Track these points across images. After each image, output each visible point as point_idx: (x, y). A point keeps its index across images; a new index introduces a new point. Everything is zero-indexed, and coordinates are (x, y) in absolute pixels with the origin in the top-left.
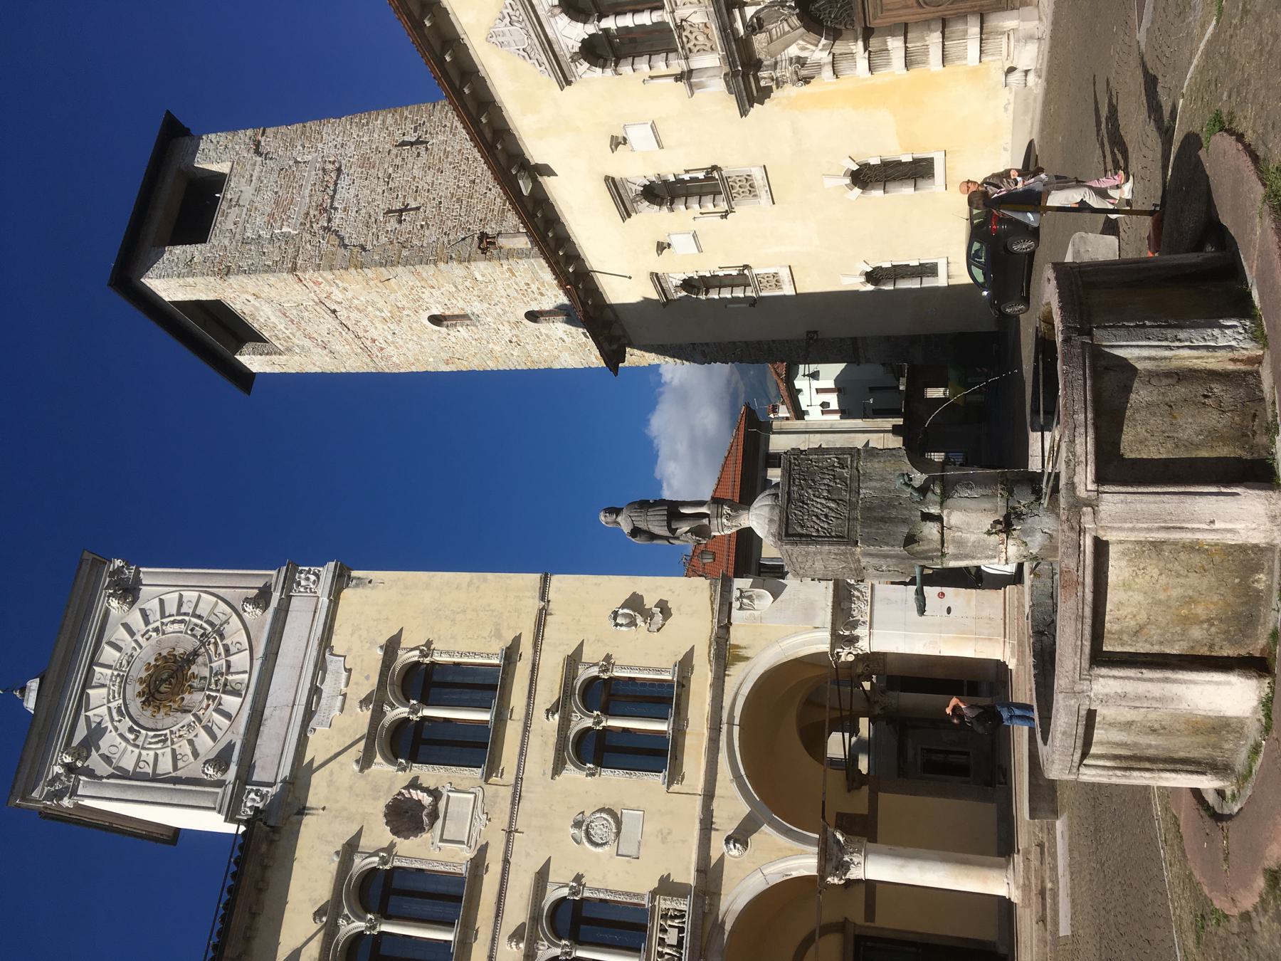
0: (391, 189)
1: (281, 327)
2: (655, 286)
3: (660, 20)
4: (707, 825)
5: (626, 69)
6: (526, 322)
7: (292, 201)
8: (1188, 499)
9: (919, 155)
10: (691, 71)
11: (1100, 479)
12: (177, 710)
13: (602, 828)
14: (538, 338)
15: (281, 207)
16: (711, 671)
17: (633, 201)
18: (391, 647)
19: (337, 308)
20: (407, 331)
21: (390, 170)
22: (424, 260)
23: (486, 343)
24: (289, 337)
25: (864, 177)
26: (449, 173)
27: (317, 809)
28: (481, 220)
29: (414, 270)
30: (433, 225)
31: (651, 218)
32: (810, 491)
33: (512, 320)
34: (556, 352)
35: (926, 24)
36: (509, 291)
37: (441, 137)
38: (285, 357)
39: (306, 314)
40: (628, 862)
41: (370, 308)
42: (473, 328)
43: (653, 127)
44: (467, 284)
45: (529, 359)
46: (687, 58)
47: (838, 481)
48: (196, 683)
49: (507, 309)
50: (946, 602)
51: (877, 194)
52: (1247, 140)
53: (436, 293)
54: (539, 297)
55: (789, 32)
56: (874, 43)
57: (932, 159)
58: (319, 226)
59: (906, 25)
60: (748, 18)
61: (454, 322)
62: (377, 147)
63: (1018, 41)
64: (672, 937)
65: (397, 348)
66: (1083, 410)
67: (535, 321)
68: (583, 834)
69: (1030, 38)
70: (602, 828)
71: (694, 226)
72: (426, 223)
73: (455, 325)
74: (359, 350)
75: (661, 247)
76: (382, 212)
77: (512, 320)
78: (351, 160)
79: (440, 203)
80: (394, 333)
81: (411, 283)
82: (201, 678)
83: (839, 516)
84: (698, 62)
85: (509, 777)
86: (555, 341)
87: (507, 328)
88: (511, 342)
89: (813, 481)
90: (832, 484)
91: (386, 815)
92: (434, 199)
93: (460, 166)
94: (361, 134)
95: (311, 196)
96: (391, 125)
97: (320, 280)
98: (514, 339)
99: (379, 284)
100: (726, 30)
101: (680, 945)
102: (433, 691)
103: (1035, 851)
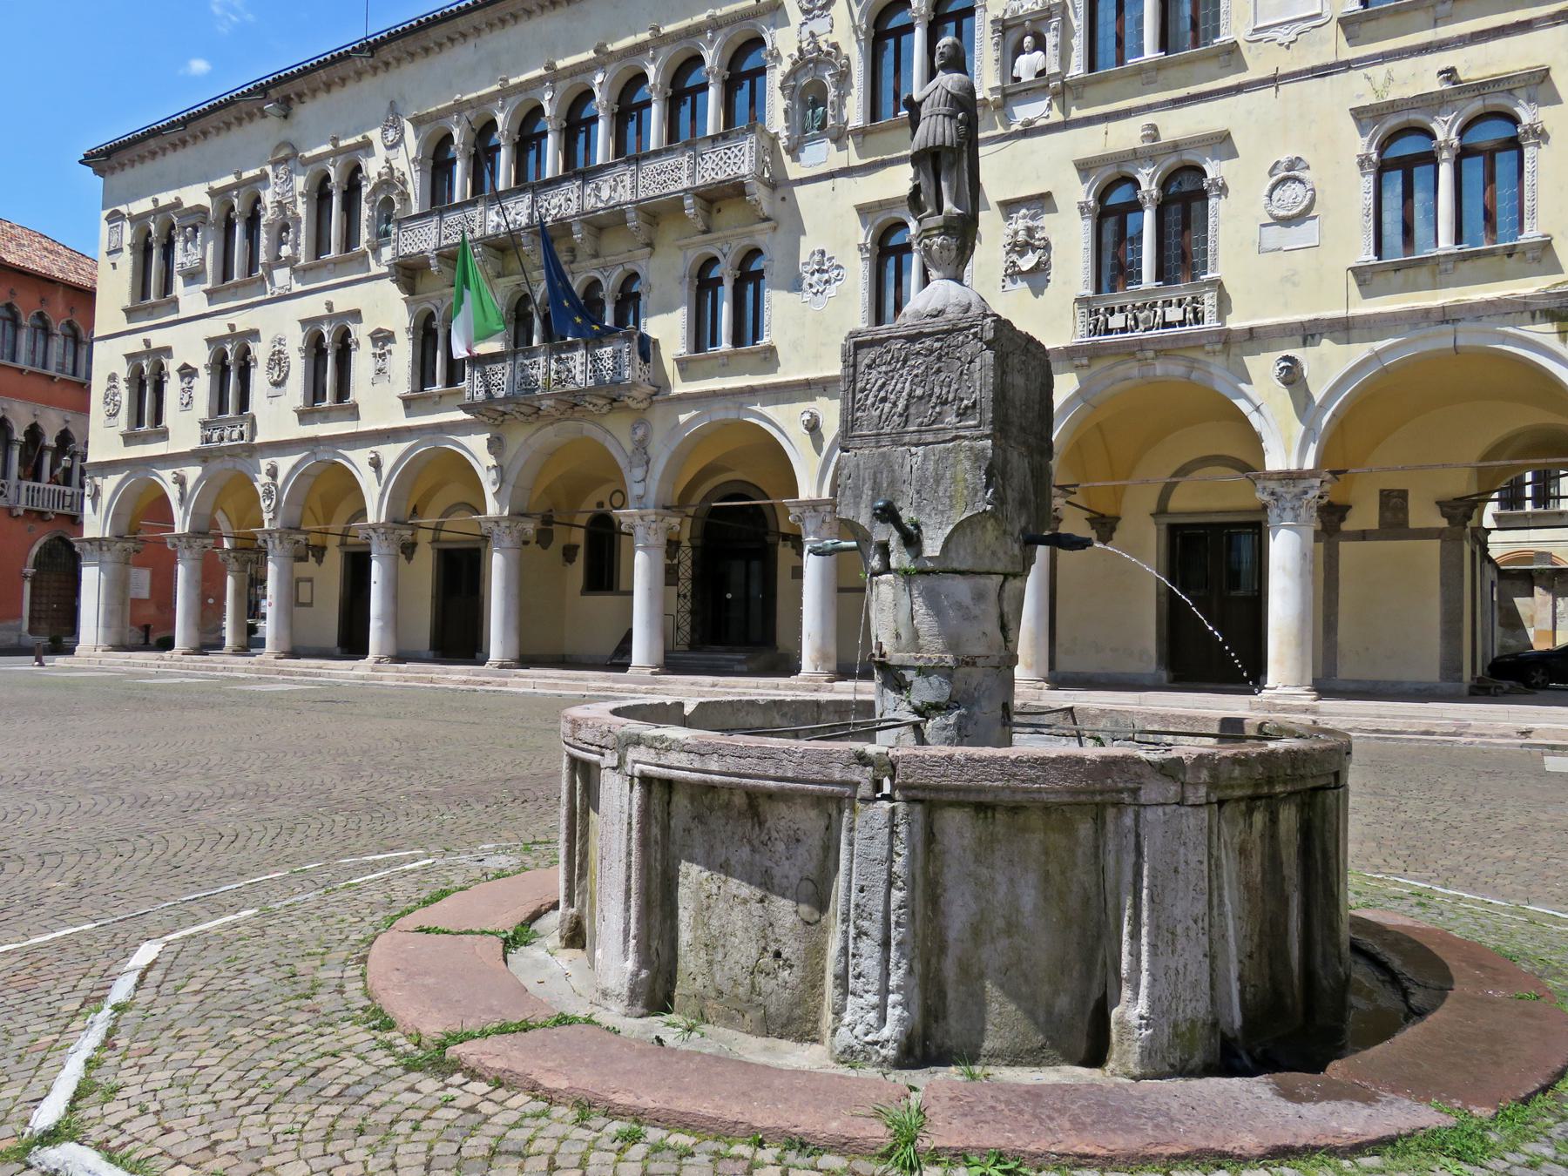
8: (621, 896)
11: (646, 781)
13: (1292, 198)
32: (923, 368)
40: (1254, 242)
47: (938, 409)
52: (484, 1127)
64: (1174, 314)
66: (724, 769)
68: (1281, 175)
70: (1292, 198)
83: (884, 417)
89: (939, 371)
90: (934, 400)
101: (1166, 325)
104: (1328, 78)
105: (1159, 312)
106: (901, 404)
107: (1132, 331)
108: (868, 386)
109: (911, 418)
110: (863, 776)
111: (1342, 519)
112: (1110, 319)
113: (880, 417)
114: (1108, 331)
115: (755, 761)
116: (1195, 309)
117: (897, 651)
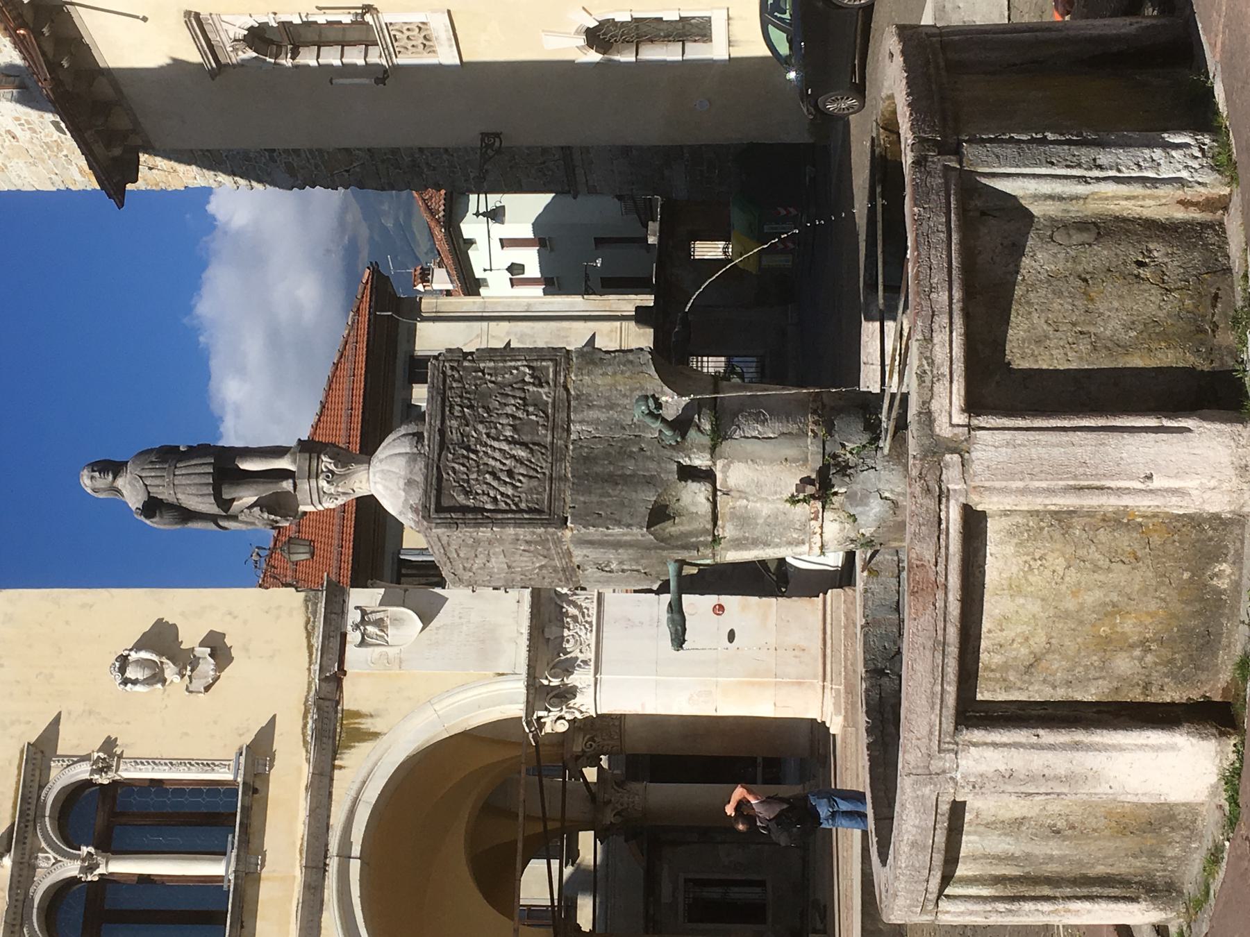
11: (974, 405)
16: (308, 760)
32: (480, 427)
47: (531, 409)
66: (946, 285)
83: (532, 473)
90: (520, 414)
106: (521, 453)
108: (492, 493)
109: (536, 439)
110: (937, 162)
113: (531, 477)
115: (933, 252)
117: (806, 460)
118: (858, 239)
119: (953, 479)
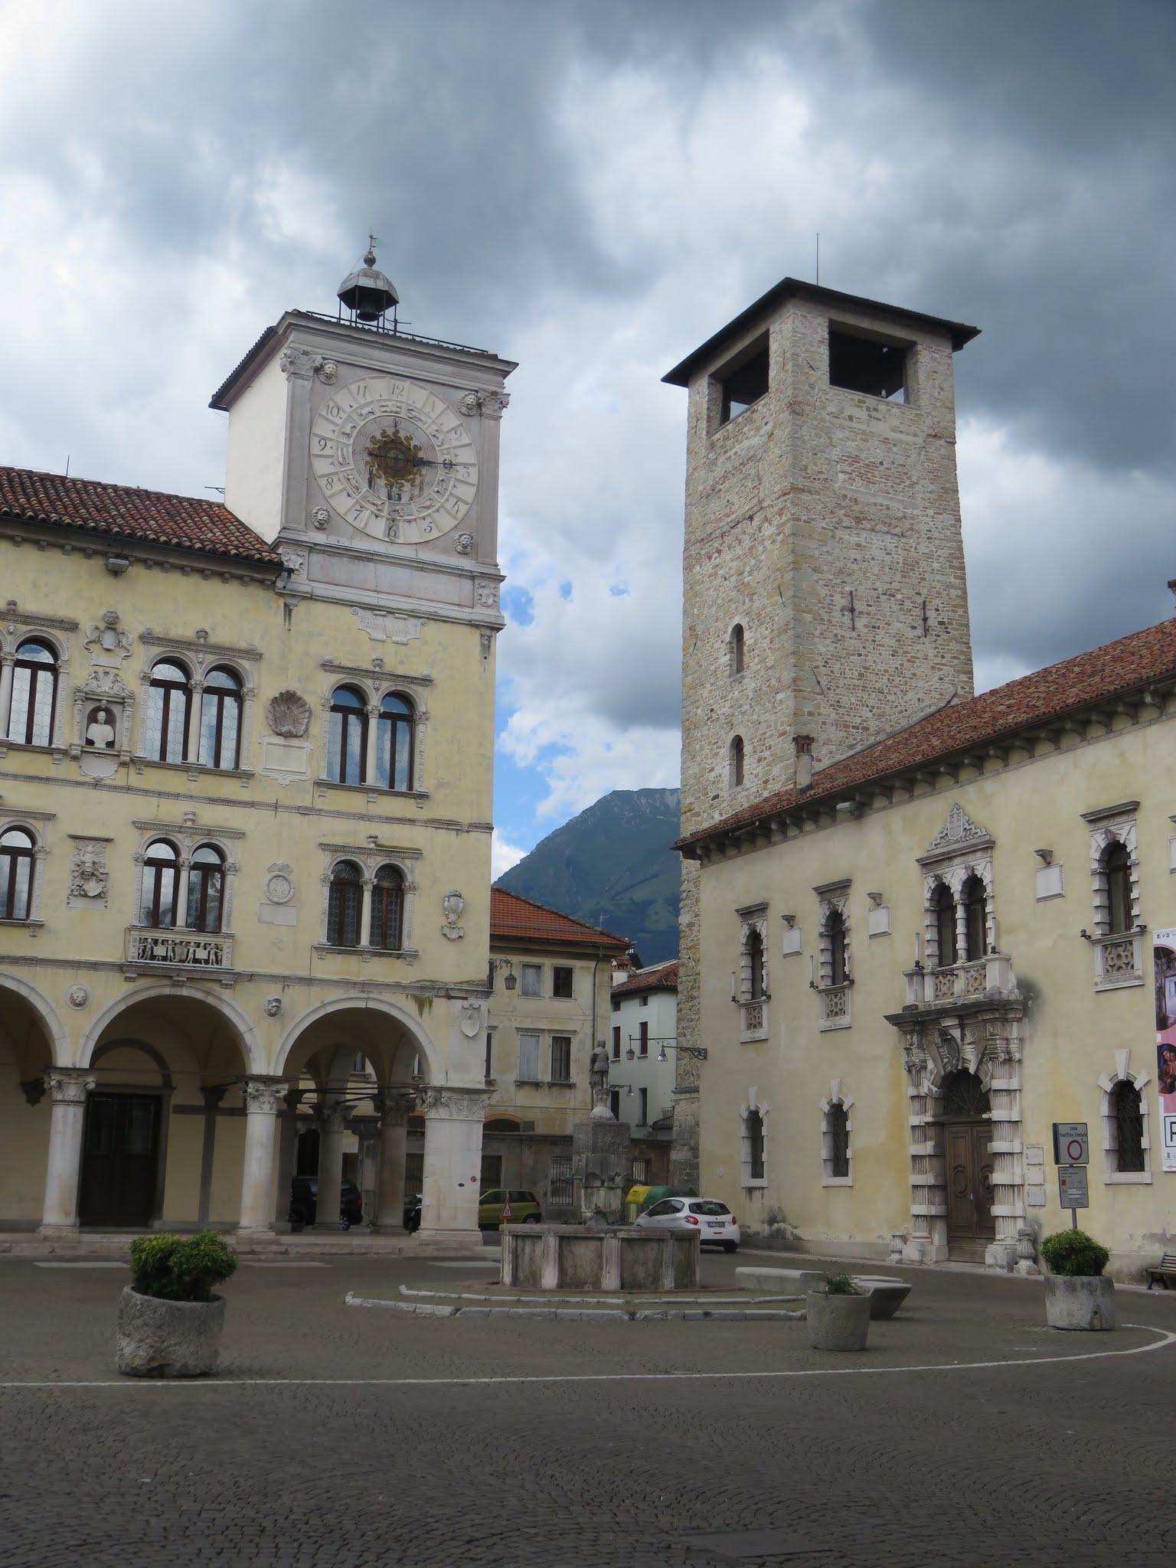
0: (878, 598)
1: (737, 448)
2: (756, 906)
3: (959, 956)
4: (285, 980)
5: (928, 920)
6: (732, 735)
7: (873, 483)
9: (851, 1163)
10: (923, 975)
11: (623, 1239)
12: (371, 473)
14: (715, 743)
15: (867, 471)
16: (411, 983)
17: (830, 903)
18: (426, 681)
19: (755, 523)
20: (728, 595)
21: (899, 596)
22: (799, 640)
23: (712, 681)
24: (726, 452)
25: (838, 1116)
26: (894, 663)
27: (290, 624)
28: (838, 702)
29: (789, 627)
30: (836, 648)
31: (814, 916)
33: (734, 719)
34: (698, 759)
35: (942, 1173)
36: (764, 725)
37: (931, 652)
38: (705, 437)
39: (750, 485)
41: (753, 562)
42: (728, 672)
43: (885, 934)
44: (773, 682)
45: (693, 726)
46: (933, 974)
48: (395, 490)
49: (746, 717)
50: (468, 1184)
51: (824, 1126)
53: (766, 644)
54: (757, 756)
55: (943, 1062)
56: (931, 1132)
57: (763, 1177)
58: (843, 517)
59: (944, 1156)
60: (951, 1032)
61: (735, 650)
62: (924, 579)
63: (922, 1245)
64: (202, 954)
65: (710, 576)
67: (732, 744)
69: (923, 1253)
71: (807, 954)
72: (839, 640)
73: (732, 652)
74: (709, 530)
75: (790, 920)
76: (853, 589)
77: (734, 719)
78: (913, 550)
79: (860, 655)
80: (725, 579)
81: (776, 618)
82: (399, 495)
84: (929, 982)
85: (319, 804)
86: (710, 761)
87: (726, 710)
88: (712, 710)
91: (288, 692)
92: (864, 648)
93: (899, 676)
94: (941, 559)
95: (875, 504)
96: (948, 595)
97: (784, 518)
98: (714, 716)
99: (777, 583)
100: (943, 1013)
101: (196, 961)
102: (389, 723)
103: (282, 1249)
104: (307, 817)
105: (191, 951)
107: (171, 961)
111: (221, 1098)
112: (155, 948)
114: (153, 957)
116: (216, 953)
118: (677, 944)
119: (609, 1235)
